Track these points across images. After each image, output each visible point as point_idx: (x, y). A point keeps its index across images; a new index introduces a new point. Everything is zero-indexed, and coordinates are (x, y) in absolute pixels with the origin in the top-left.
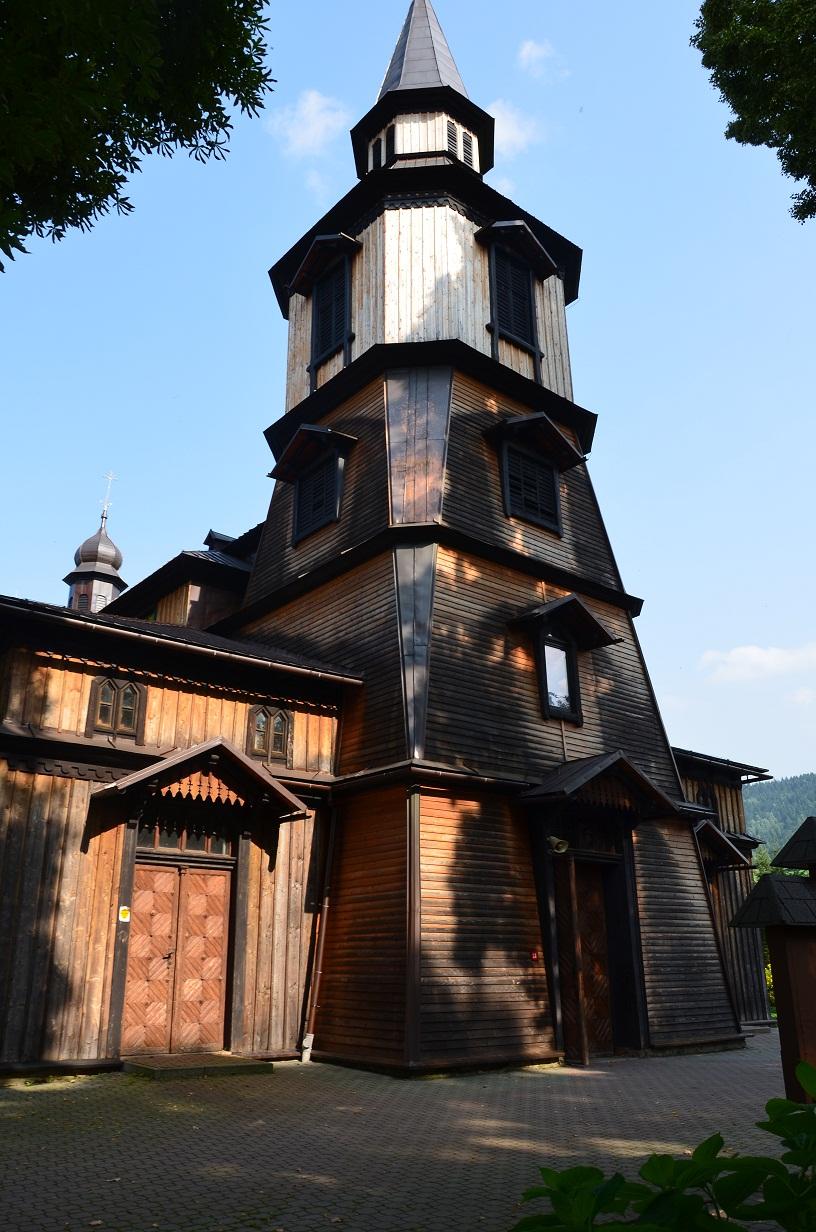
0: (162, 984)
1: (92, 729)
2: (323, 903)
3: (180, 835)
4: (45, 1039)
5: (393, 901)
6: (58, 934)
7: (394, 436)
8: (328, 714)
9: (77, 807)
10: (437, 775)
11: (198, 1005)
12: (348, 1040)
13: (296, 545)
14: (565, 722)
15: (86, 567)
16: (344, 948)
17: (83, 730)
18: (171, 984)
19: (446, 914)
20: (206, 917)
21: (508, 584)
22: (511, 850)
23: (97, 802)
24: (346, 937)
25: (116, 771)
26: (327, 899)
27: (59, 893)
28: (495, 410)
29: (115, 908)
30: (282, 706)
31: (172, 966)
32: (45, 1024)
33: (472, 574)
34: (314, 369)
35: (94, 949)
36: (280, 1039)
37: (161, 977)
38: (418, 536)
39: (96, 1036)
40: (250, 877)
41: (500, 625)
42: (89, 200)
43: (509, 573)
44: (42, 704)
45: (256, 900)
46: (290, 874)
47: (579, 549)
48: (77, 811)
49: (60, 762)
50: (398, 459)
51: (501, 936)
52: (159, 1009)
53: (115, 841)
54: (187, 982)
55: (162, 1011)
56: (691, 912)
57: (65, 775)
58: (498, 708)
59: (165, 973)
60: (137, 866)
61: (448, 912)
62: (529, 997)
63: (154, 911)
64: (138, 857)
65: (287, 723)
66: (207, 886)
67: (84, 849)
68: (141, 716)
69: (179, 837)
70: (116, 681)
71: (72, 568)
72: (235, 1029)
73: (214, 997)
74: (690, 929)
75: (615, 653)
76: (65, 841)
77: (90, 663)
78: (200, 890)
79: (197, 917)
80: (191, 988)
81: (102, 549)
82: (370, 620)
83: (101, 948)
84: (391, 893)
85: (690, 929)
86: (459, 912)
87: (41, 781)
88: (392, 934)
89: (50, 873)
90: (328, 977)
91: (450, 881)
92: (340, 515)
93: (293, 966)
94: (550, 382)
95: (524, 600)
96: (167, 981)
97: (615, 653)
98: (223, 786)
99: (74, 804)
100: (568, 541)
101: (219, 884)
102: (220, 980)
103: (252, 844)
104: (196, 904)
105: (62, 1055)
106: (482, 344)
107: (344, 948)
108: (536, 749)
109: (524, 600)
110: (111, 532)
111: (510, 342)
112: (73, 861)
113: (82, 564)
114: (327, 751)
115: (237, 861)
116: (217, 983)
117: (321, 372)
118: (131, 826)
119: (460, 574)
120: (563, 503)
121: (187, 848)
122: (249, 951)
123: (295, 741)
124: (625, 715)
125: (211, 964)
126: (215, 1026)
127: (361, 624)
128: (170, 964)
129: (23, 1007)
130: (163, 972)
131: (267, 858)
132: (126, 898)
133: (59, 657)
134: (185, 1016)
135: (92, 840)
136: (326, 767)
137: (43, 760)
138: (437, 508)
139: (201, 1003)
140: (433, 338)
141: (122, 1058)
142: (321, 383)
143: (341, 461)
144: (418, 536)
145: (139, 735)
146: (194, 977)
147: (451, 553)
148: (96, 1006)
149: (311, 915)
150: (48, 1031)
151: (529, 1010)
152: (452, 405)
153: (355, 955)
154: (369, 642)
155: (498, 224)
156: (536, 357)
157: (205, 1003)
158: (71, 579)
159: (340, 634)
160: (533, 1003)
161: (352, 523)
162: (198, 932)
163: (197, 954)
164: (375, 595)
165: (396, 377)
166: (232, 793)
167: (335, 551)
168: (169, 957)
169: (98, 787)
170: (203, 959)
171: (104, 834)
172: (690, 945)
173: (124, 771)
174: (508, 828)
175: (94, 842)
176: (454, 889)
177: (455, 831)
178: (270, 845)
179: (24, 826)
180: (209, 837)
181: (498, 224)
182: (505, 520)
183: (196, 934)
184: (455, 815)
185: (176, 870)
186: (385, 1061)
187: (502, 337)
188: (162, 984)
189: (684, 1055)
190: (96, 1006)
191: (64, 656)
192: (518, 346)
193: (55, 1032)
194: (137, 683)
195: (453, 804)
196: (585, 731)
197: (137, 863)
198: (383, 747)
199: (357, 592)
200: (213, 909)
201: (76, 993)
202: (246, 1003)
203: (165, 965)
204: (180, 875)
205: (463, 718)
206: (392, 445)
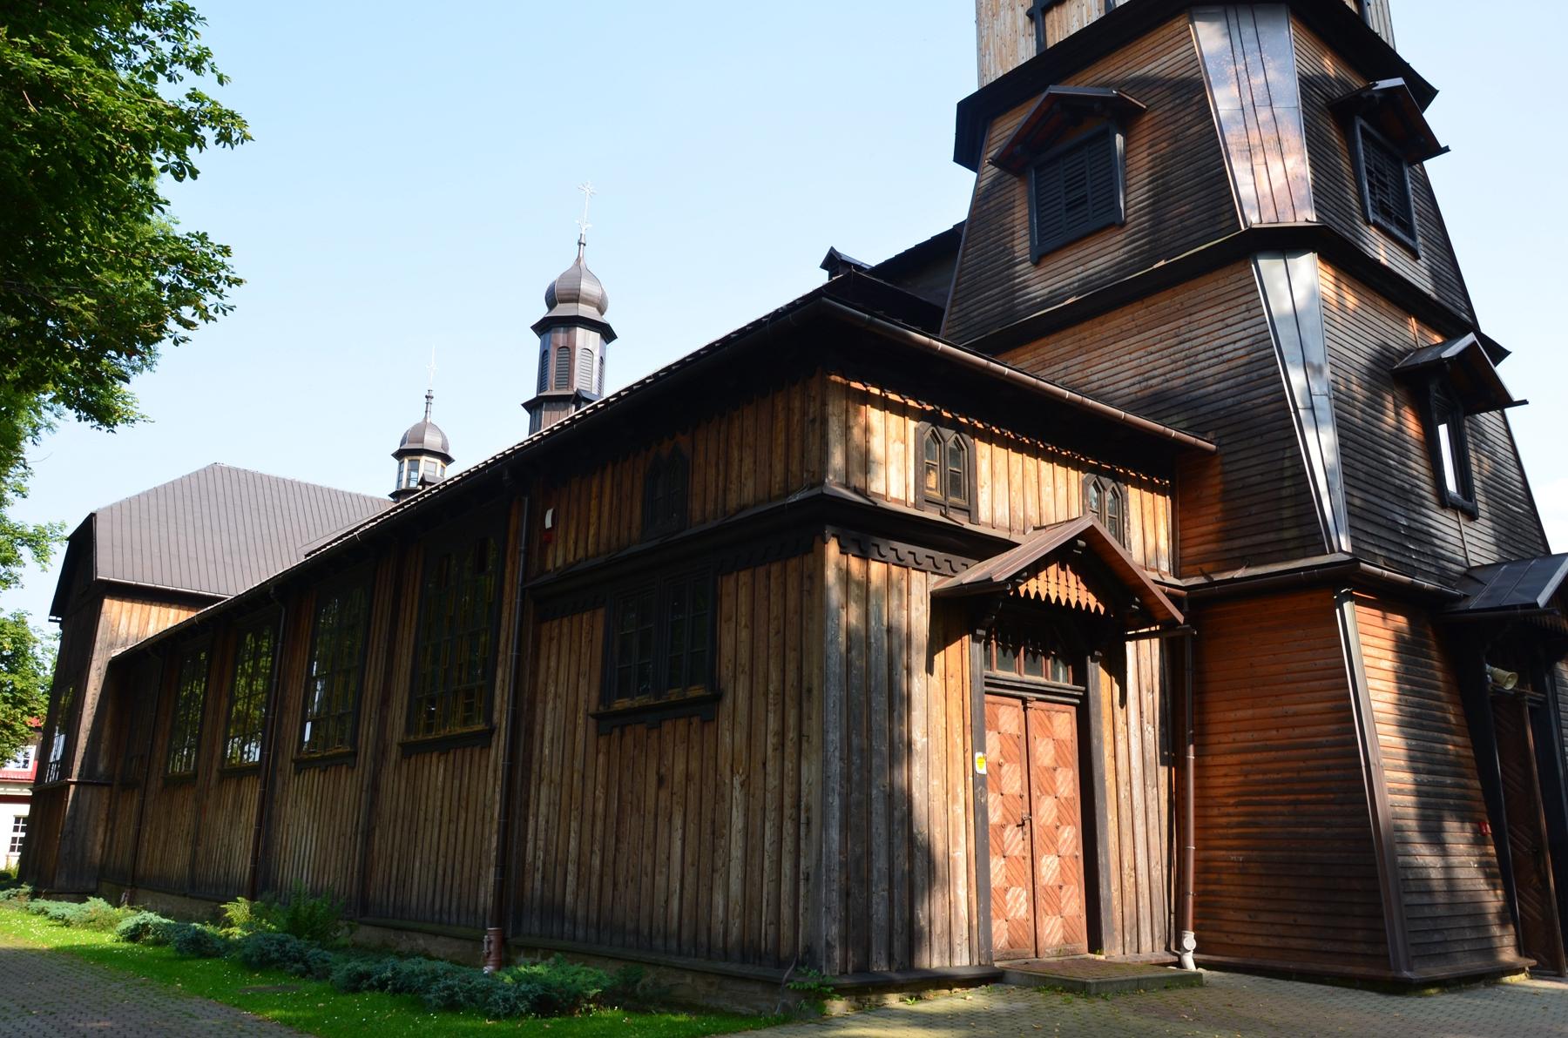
0: (1019, 862)
1: (924, 500)
2: (1186, 753)
3: (1016, 654)
4: (912, 937)
5: (1327, 750)
6: (914, 789)
7: (1224, 101)
8: (1162, 491)
9: (917, 609)
11: (1058, 890)
12: (1260, 941)
13: (1037, 261)
14: (1462, 512)
15: (562, 310)
16: (1228, 815)
17: (912, 500)
18: (1029, 861)
19: (1402, 770)
20: (1055, 770)
21: (1383, 318)
22: (1440, 684)
23: (941, 604)
24: (1232, 801)
25: (957, 560)
26: (1191, 748)
27: (909, 732)
28: (1332, 73)
29: (969, 754)
30: (1116, 477)
31: (1028, 836)
32: (911, 920)
33: (1351, 300)
35: (953, 812)
36: (1149, 939)
37: (1016, 853)
38: (1285, 242)
39: (966, 935)
40: (1102, 715)
41: (1384, 373)
43: (1383, 304)
44: (864, 461)
46: (1141, 713)
47: (1435, 276)
48: (918, 618)
49: (896, 545)
50: (1236, 133)
51: (1451, 802)
52: (1019, 896)
53: (962, 655)
54: (1043, 860)
55: (1022, 899)
57: (900, 563)
58: (1402, 488)
59: (1021, 846)
60: (989, 698)
61: (1401, 766)
62: (1488, 885)
63: (1002, 760)
64: (987, 684)
65: (1120, 500)
66: (1052, 726)
67: (930, 669)
68: (972, 481)
69: (1015, 657)
70: (942, 430)
71: (542, 312)
72: (1106, 925)
73: (1073, 880)
75: (1487, 423)
76: (909, 657)
77: (911, 403)
78: (1048, 732)
79: (1047, 769)
80: (1049, 867)
81: (586, 287)
82: (1215, 360)
83: (960, 810)
84: (1319, 739)
86: (1413, 768)
87: (877, 568)
88: (1332, 796)
89: (898, 702)
90: (1203, 854)
91: (1401, 724)
92: (1126, 217)
93: (1154, 840)
95: (1400, 342)
96: (1024, 858)
97: (1487, 423)
98: (1082, 586)
99: (913, 606)
100: (1424, 265)
101: (1064, 722)
102: (1077, 857)
103: (1101, 669)
104: (1044, 752)
105: (933, 960)
107: (1228, 815)
108: (1442, 548)
109: (1400, 342)
110: (590, 262)
112: (921, 687)
113: (559, 305)
114: (1164, 544)
115: (1086, 692)
116: (1074, 860)
118: (976, 639)
119: (1340, 300)
121: (1025, 673)
122: (1110, 817)
123: (1131, 527)
124: (1507, 507)
125: (1066, 835)
126: (1076, 920)
127: (1195, 367)
128: (1025, 834)
129: (886, 894)
130: (1017, 845)
131: (1117, 688)
132: (980, 745)
133: (876, 391)
134: (1046, 907)
135: (936, 657)
136: (1165, 566)
137: (877, 540)
138: (1306, 202)
139: (1061, 887)
141: (997, 965)
142: (1055, 36)
143: (1119, 139)
144: (1285, 242)
145: (973, 509)
146: (1049, 852)
147: (1329, 269)
148: (962, 892)
149: (1166, 769)
150: (916, 926)
151: (1493, 901)
153: (1256, 825)
154: (1216, 392)
157: (1065, 888)
158: (543, 328)
159: (1153, 382)
160: (1492, 892)
161: (1151, 227)
162: (1050, 790)
163: (1050, 821)
164: (1220, 325)
165: (1207, 18)
166: (1091, 596)
167: (1121, 268)
168: (1023, 824)
169: (937, 582)
170: (1057, 827)
171: (948, 648)
173: (964, 560)
174: (1434, 654)
175: (939, 659)
176: (1407, 736)
177: (1390, 655)
178: (1118, 671)
179: (863, 633)
180: (1047, 658)
182: (1365, 228)
183: (1047, 793)
184: (1389, 634)
185: (1019, 702)
186: (1361, 970)
188: (1019, 862)
190: (962, 892)
191: (882, 391)
193: (922, 929)
194: (964, 435)
195: (1384, 618)
196: (1478, 527)
197: (987, 693)
198: (1272, 536)
199: (1182, 322)
200: (1061, 758)
201: (940, 873)
202: (1113, 888)
203: (1020, 835)
204: (1025, 709)
206: (1221, 113)
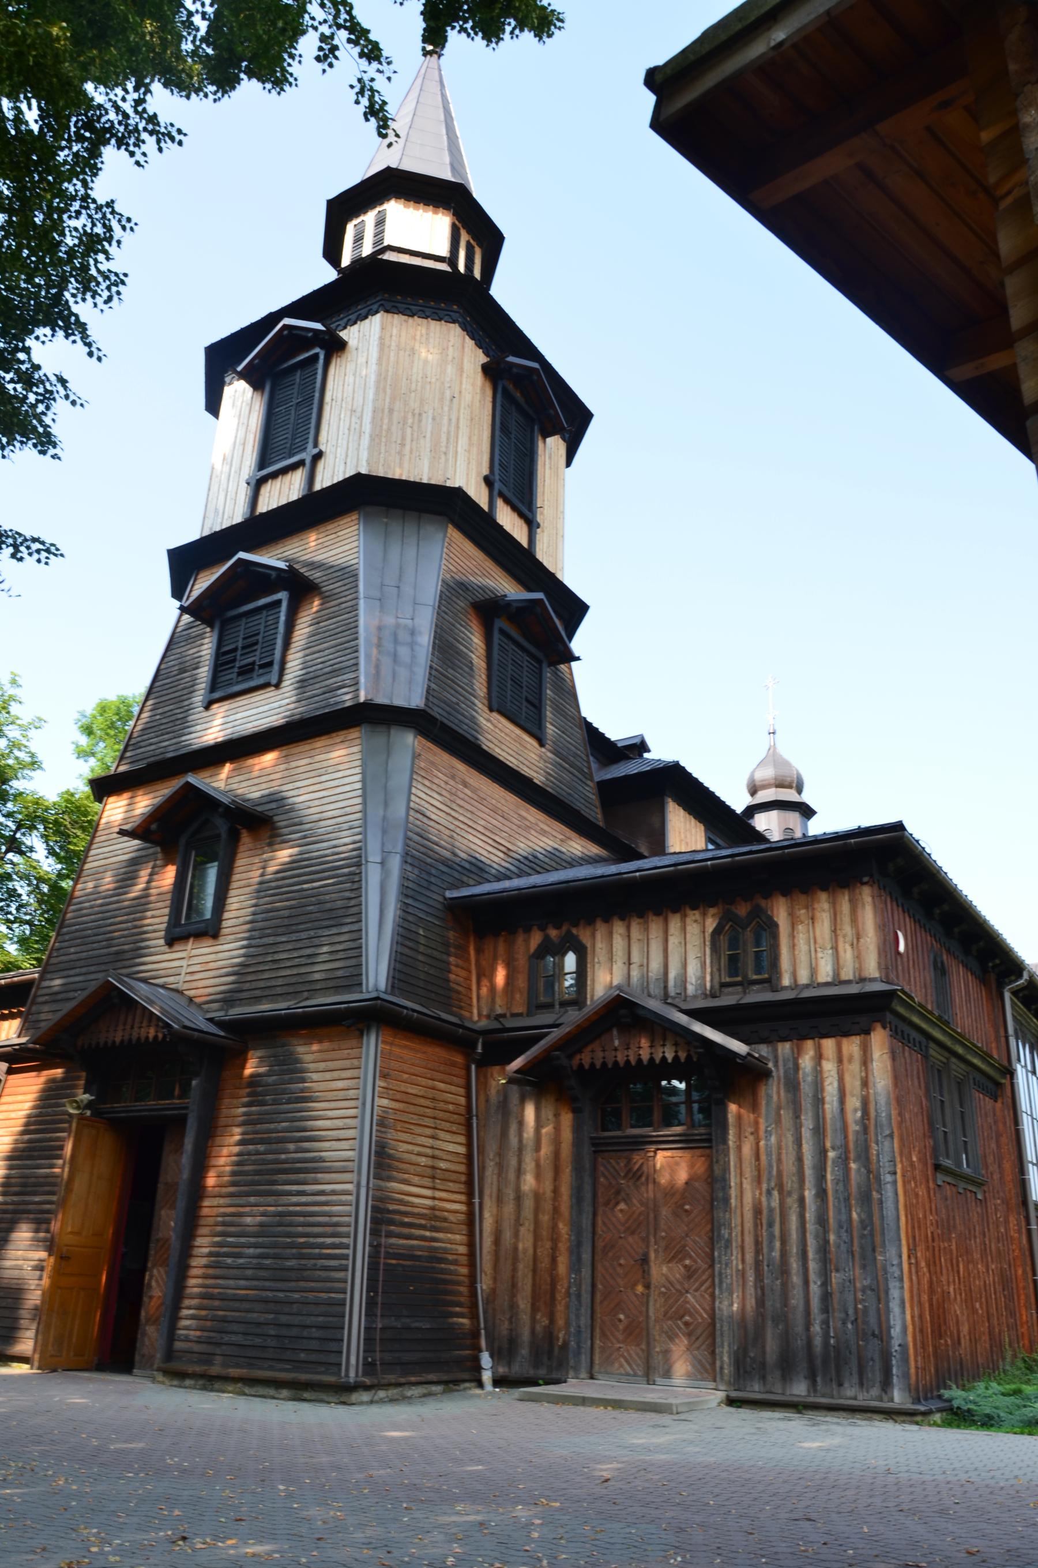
10: (280, 1015)
34: (257, 485)
42: (39, 174)
45: (334, 1143)
56: (315, 1171)
74: (303, 1199)
85: (303, 1199)
94: (543, 555)
106: (479, 495)
111: (507, 501)
117: (266, 490)
120: (481, 680)
140: (418, 480)
142: (263, 508)
152: (444, 561)
155: (511, 359)
156: (531, 524)
172: (291, 1225)
181: (511, 359)
187: (501, 495)
189: (212, 1390)
192: (514, 508)
205: (77, 979)
